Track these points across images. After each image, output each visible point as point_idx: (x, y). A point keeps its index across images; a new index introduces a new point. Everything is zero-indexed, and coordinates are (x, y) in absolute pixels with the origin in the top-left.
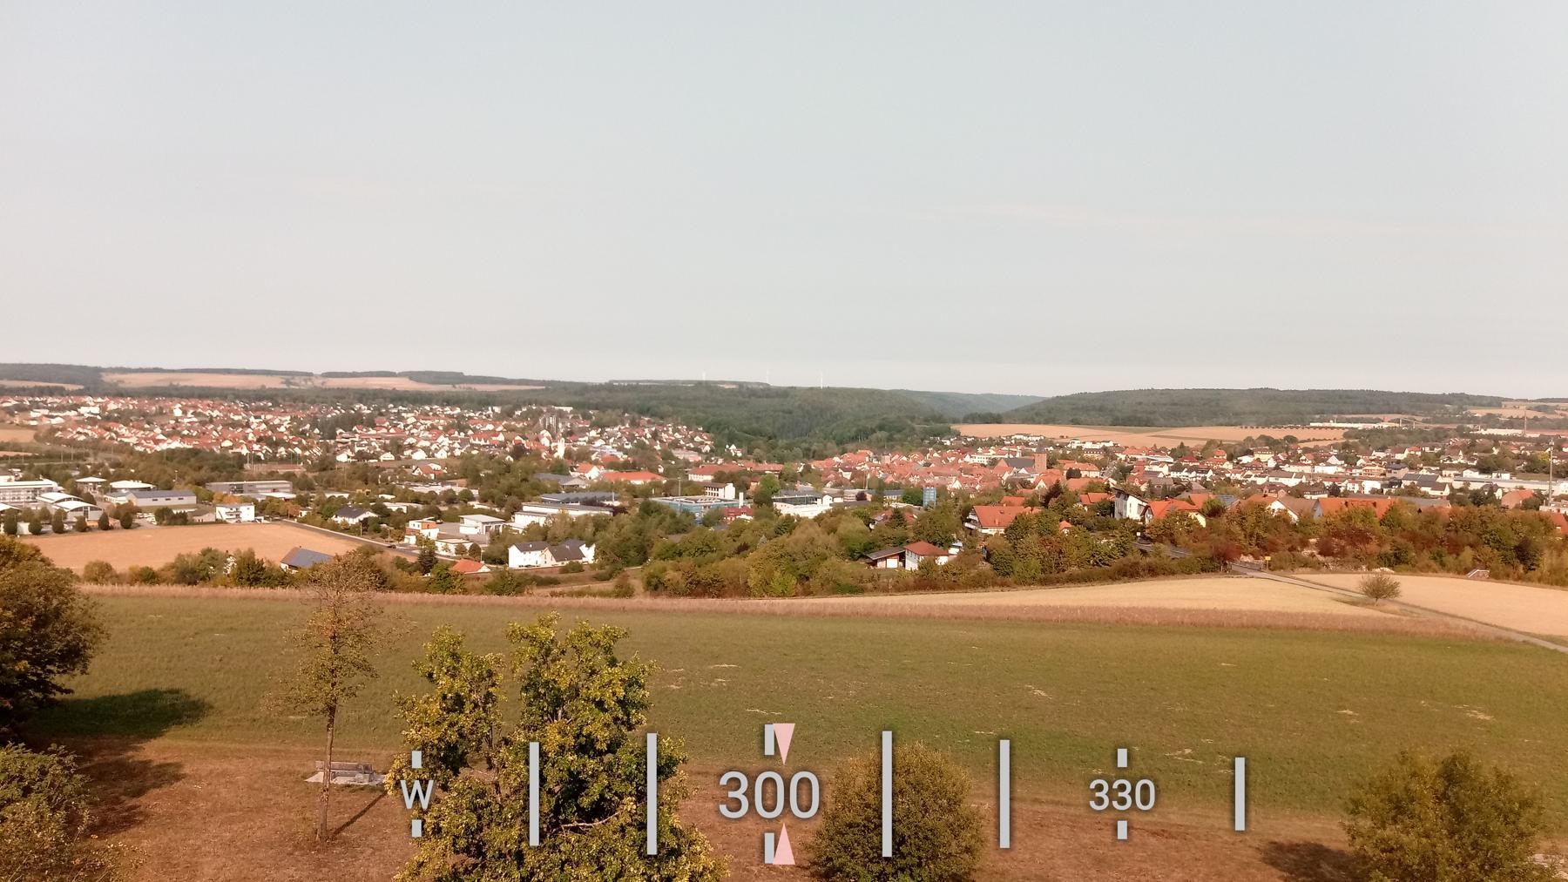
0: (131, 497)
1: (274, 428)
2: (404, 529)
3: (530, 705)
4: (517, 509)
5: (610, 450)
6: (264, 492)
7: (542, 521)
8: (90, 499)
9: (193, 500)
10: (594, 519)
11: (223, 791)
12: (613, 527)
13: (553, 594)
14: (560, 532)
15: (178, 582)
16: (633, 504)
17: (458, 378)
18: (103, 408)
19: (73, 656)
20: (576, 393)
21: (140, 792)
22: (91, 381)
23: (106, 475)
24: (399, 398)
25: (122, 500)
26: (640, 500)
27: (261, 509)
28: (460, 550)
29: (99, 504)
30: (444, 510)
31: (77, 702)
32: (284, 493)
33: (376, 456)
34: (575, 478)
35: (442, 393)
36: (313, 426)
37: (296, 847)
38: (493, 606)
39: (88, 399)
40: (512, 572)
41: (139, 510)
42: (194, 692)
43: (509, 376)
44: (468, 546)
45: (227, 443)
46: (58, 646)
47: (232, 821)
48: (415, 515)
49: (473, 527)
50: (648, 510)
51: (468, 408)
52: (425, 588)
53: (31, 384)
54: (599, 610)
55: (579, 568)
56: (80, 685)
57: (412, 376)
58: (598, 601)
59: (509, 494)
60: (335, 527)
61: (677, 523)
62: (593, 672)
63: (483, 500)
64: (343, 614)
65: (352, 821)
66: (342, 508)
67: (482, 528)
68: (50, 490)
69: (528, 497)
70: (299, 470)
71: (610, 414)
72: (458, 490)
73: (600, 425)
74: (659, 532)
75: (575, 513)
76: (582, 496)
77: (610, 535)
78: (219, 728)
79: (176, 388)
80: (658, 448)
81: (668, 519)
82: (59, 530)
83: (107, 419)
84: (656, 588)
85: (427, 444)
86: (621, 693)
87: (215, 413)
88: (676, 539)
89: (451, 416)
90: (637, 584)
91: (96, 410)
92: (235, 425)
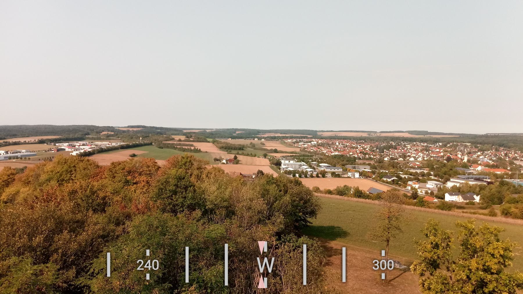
0: (325, 168)
1: (365, 149)
2: (406, 184)
3: (464, 251)
4: (449, 180)
5: (486, 160)
6: (362, 169)
7: (458, 185)
8: (314, 168)
9: (341, 170)
10: (479, 185)
11: (354, 261)
12: (487, 189)
13: (463, 212)
14: (465, 190)
15: (337, 194)
16: (496, 181)
17: (426, 133)
18: (318, 142)
19: (313, 213)
20: (472, 138)
21: (330, 256)
22: (314, 134)
23: (318, 162)
24: (405, 140)
25: (322, 169)
26: (499, 180)
27: (361, 174)
28: (427, 193)
29: (316, 170)
30: (422, 179)
31: (312, 226)
32: (368, 169)
33: (397, 159)
34: (471, 170)
35: (420, 138)
36: (377, 148)
37: (377, 283)
38: (440, 214)
39: (314, 140)
40: (446, 202)
41: (327, 172)
42: (345, 228)
43: (445, 132)
44: (429, 192)
45: (351, 153)
46: (309, 210)
47: (357, 270)
48: (410, 180)
49: (431, 185)
50: (502, 184)
51: (430, 144)
52: (415, 205)
53: (291, 135)
54: (479, 220)
55: (473, 204)
56: (315, 222)
57: (128, 127)
58: (482, 217)
59: (445, 174)
60: (384, 181)
61: (516, 189)
62: (489, 243)
63: (435, 176)
64: (391, 210)
65: (395, 278)
66: (386, 175)
67: (434, 186)
68: (304, 165)
69: (452, 176)
70: (372, 162)
71: (486, 146)
72: (426, 172)
73: (482, 150)
74: (508, 192)
75: (472, 183)
76: (474, 176)
77: (486, 192)
78: (352, 241)
79: (337, 136)
80: (507, 160)
81: (512, 188)
82: (306, 177)
83: (319, 145)
84: (506, 214)
85: (415, 155)
86: (502, 252)
87: (348, 144)
88: (516, 196)
89: (423, 146)
90: (498, 212)
91: (316, 143)
92: (353, 148)
